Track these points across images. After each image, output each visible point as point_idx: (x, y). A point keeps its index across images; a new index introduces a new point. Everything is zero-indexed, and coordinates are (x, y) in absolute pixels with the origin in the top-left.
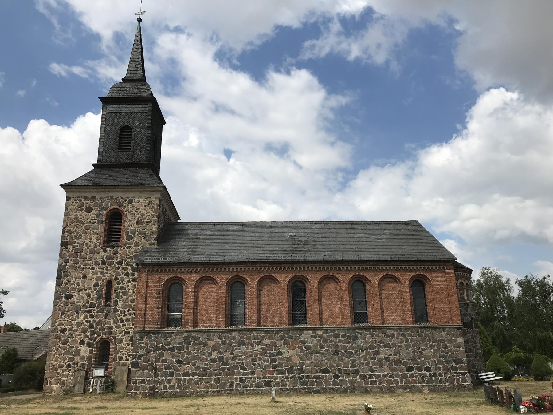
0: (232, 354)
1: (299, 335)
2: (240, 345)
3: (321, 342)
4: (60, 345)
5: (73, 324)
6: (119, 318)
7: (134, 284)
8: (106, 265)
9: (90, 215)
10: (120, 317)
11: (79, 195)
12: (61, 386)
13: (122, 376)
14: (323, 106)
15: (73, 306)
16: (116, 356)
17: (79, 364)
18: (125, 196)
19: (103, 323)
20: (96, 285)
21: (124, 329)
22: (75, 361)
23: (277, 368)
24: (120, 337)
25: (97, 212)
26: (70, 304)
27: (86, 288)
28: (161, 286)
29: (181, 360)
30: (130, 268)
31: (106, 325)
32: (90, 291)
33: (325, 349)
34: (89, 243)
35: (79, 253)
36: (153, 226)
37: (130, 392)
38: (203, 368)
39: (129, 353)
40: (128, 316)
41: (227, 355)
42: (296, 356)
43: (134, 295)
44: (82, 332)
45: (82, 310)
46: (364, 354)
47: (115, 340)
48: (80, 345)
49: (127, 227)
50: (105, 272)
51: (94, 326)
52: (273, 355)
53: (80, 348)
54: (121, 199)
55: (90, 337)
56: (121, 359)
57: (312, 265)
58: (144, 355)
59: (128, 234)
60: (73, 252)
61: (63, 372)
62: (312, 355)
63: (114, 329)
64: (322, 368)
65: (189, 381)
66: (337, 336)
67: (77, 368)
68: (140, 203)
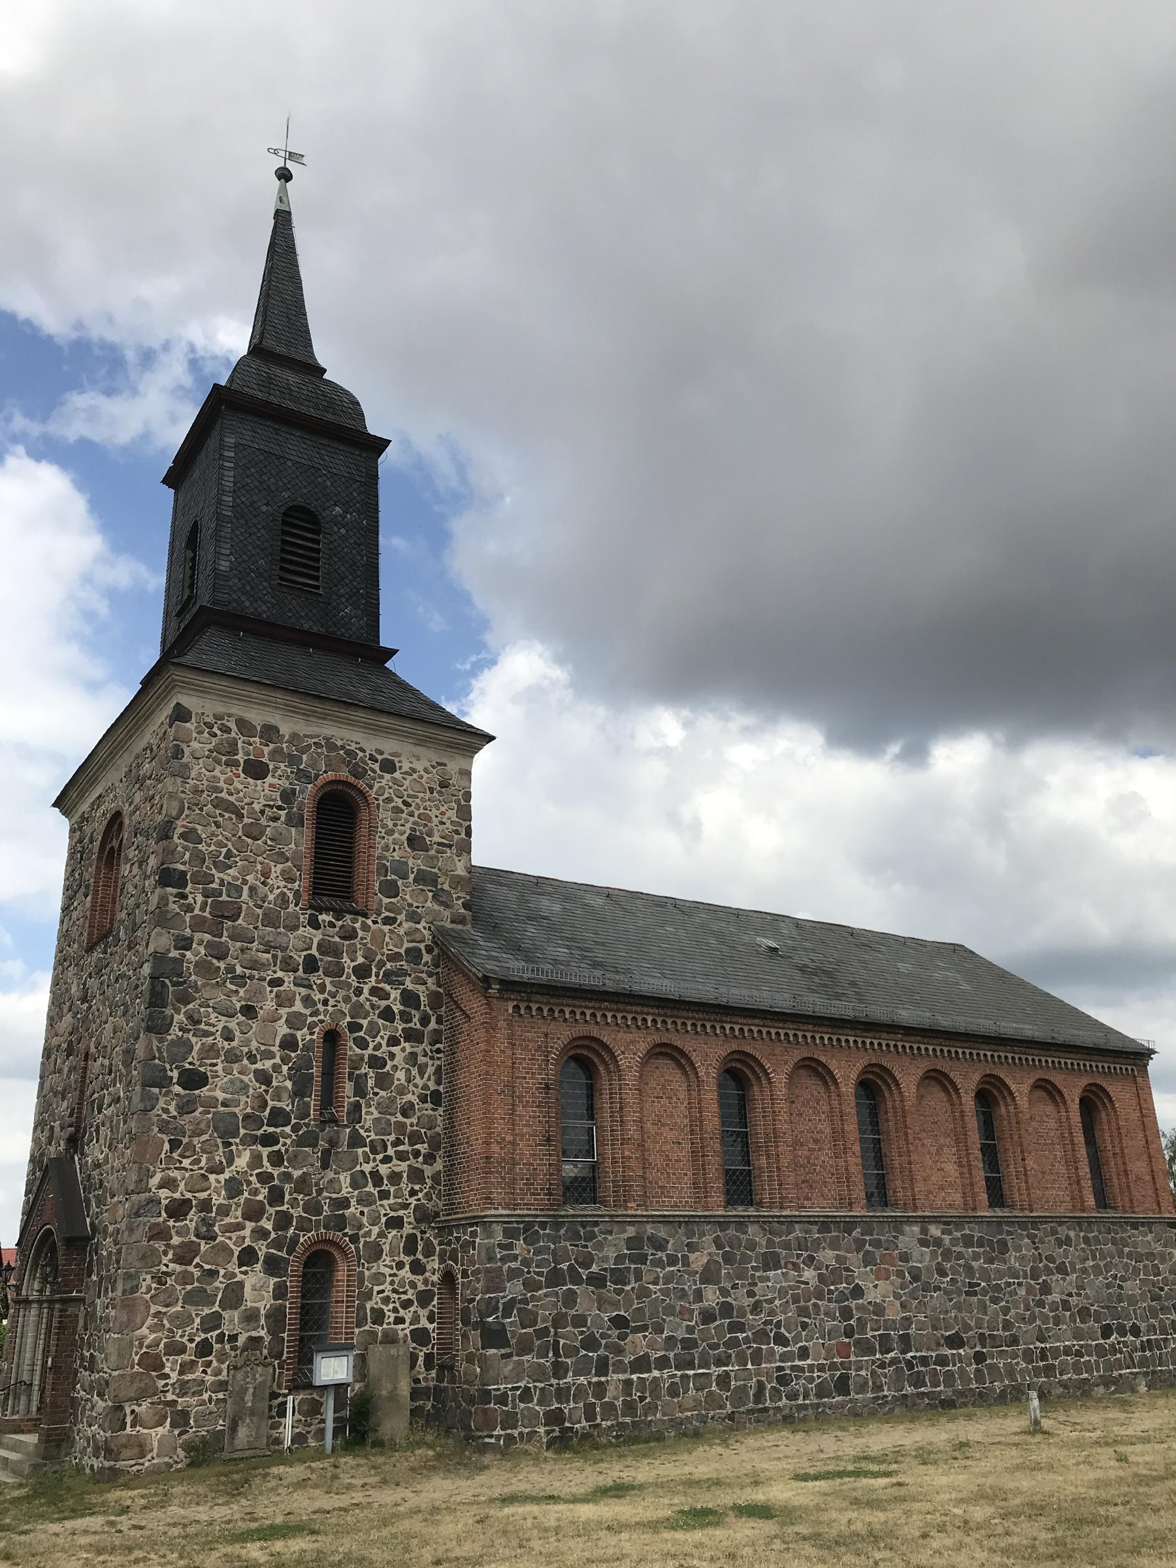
0: (751, 1294)
1: (895, 1237)
2: (767, 1268)
3: (940, 1259)
4: (168, 1265)
5: (214, 1184)
6: (367, 1168)
7: (408, 1050)
8: (321, 972)
9: (259, 788)
10: (372, 1164)
11: (221, 708)
12: (176, 1432)
13: (395, 1380)
14: (87, 579)
15: (210, 1116)
16: (362, 1307)
17: (241, 1340)
18: (371, 744)
19: (317, 1184)
20: (289, 1043)
21: (384, 1208)
22: (226, 1329)
23: (857, 1336)
24: (373, 1237)
25: (285, 783)
26: (201, 1109)
27: (254, 1052)
28: (699, 1067)
29: (626, 1315)
30: (395, 994)
31: (325, 1194)
32: (268, 1064)
33: (948, 1279)
34: (263, 890)
35: (227, 918)
36: (456, 859)
37: (491, 1436)
38: (683, 1340)
39: (404, 1297)
40: (395, 1161)
41: (740, 1299)
42: (892, 1299)
43: (411, 1088)
44: (247, 1216)
45: (242, 1131)
46: (1022, 1292)
47: (357, 1249)
48: (240, 1266)
49: (380, 851)
50: (316, 998)
51: (287, 1197)
52: (843, 1297)
53: (240, 1277)
54: (361, 754)
55: (273, 1235)
56: (378, 1317)
57: (905, 1038)
58: (521, 1302)
59: (386, 876)
60: (207, 914)
61: (181, 1373)
62: (925, 1297)
63: (352, 1209)
64: (948, 1334)
65: (653, 1386)
66: (968, 1241)
67: (233, 1353)
68: (415, 776)
